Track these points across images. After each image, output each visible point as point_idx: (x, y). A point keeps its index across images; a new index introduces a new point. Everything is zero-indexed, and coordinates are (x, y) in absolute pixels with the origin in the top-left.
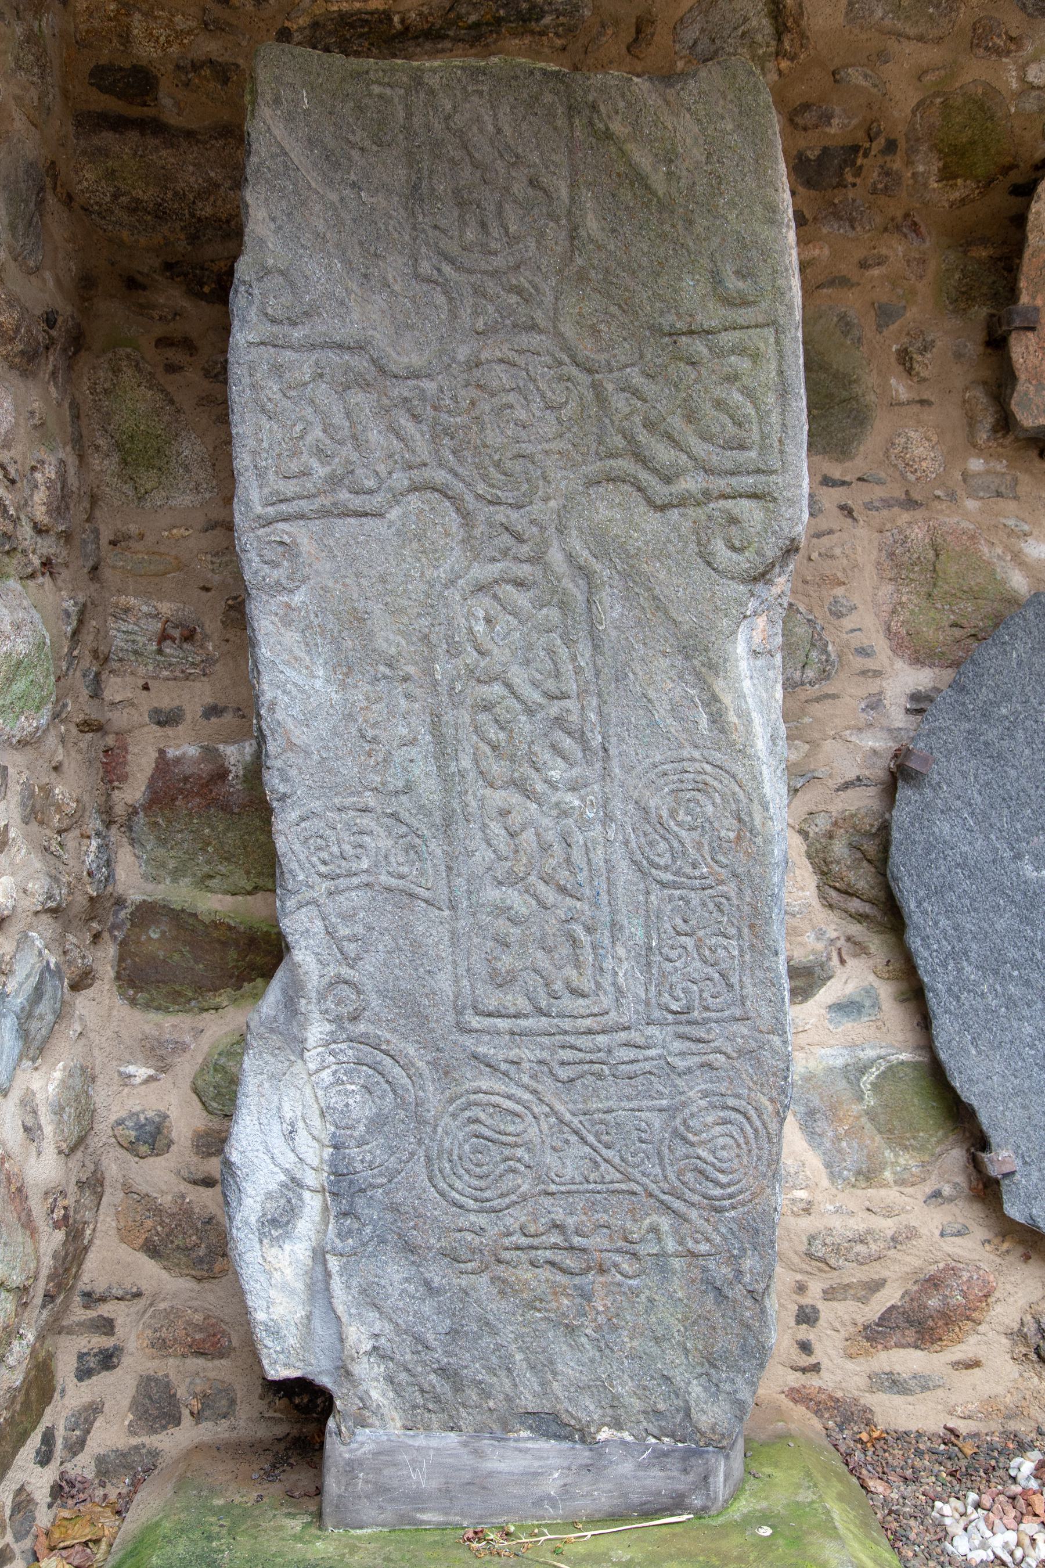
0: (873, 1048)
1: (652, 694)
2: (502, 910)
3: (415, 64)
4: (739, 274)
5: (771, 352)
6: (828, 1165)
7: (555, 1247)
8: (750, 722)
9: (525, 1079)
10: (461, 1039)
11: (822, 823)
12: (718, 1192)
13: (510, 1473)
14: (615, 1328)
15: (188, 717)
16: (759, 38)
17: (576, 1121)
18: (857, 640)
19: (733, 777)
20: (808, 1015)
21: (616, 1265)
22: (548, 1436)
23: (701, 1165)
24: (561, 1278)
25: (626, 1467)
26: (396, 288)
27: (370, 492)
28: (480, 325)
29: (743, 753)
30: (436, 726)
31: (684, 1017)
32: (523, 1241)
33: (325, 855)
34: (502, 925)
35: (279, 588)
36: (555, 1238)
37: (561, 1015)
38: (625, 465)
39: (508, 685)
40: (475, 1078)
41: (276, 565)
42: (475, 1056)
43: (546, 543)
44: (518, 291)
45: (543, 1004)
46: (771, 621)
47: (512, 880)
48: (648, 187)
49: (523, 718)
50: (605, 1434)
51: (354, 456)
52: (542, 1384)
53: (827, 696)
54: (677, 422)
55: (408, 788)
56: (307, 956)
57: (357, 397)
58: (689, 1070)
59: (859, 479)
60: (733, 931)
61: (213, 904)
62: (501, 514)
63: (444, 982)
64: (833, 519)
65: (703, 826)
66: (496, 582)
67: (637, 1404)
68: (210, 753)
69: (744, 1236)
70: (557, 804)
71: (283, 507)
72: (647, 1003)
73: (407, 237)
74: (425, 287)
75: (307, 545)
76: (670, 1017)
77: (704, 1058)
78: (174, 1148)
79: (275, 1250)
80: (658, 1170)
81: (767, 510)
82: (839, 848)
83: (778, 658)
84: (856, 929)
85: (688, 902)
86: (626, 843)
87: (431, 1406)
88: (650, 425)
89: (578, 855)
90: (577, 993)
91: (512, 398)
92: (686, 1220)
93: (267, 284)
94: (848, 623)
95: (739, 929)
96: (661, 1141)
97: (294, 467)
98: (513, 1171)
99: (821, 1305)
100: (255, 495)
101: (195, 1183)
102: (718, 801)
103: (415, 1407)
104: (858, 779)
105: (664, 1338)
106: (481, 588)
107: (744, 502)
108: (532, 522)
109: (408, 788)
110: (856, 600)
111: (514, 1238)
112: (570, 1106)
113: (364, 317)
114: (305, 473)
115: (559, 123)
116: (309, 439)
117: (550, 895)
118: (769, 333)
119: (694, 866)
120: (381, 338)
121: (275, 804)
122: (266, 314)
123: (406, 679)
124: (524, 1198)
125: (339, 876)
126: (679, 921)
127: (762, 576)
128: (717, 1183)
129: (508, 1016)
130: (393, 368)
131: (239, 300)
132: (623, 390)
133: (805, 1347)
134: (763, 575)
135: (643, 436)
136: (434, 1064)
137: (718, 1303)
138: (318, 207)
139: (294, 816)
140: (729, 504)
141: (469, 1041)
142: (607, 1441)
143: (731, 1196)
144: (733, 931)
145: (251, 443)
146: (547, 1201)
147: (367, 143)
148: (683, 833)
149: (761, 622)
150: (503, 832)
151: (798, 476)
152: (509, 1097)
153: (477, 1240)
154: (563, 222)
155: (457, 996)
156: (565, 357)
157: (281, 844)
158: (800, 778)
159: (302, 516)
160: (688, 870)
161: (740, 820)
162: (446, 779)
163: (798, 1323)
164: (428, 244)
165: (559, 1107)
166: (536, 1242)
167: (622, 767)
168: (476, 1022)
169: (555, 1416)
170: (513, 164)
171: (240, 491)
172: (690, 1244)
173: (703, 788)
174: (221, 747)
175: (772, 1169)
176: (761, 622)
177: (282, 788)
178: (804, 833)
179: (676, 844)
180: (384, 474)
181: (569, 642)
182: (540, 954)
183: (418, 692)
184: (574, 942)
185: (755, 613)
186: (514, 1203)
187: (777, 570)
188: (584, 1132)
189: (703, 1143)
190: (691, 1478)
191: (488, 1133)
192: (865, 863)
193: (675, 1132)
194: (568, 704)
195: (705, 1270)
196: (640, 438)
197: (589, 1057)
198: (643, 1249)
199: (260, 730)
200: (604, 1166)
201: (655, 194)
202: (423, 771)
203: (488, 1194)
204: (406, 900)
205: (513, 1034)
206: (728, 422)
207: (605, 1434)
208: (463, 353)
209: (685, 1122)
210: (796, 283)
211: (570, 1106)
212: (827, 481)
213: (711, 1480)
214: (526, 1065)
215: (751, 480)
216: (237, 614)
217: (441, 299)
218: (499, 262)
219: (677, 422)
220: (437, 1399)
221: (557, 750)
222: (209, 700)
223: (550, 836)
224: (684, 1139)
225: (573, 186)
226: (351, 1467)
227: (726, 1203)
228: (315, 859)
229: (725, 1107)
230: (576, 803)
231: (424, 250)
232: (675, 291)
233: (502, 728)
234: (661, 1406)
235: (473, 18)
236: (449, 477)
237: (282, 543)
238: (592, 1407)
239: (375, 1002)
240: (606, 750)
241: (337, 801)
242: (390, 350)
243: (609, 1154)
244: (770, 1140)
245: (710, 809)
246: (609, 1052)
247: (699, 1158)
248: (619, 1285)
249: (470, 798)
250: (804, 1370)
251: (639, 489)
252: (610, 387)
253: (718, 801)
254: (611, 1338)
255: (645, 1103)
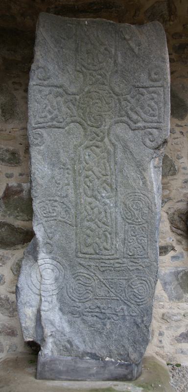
0: (182, 268)
1: (129, 176)
2: (88, 228)
3: (78, 19)
4: (155, 74)
5: (162, 93)
6: (169, 297)
7: (97, 312)
8: (153, 184)
9: (92, 270)
10: (77, 259)
11: (172, 211)
12: (139, 300)
13: (83, 368)
14: (111, 333)
15: (15, 176)
16: (165, 16)
17: (104, 281)
18: (183, 165)
19: (148, 197)
20: (166, 259)
21: (112, 317)
22: (93, 359)
23: (135, 294)
24: (98, 320)
25: (112, 368)
26: (71, 73)
27: (61, 122)
28: (91, 83)
29: (151, 191)
30: (74, 180)
31: (132, 257)
32: (90, 310)
33: (45, 212)
34: (88, 232)
35: (37, 145)
36: (97, 310)
37: (102, 255)
38: (125, 118)
39: (93, 172)
40: (79, 269)
41: (37, 139)
42: (80, 264)
43: (104, 137)
44: (101, 75)
45: (98, 252)
46: (160, 160)
47: (92, 220)
48: (134, 52)
49: (96, 180)
50: (107, 359)
51: (58, 113)
52: (93, 346)
53: (175, 179)
54: (138, 109)
55: (67, 196)
56: (39, 232)
57: (59, 99)
58: (133, 270)
59: (185, 125)
60: (146, 236)
61: (19, 223)
62: (94, 129)
63: (73, 245)
64: (178, 135)
65: (140, 210)
66: (91, 146)
67: (116, 352)
68: (20, 185)
69: (145, 312)
70: (104, 202)
71: (39, 125)
72: (123, 253)
73: (74, 61)
74: (78, 73)
75: (45, 135)
76: (129, 256)
77: (137, 267)
78: (5, 283)
79: (28, 309)
80: (124, 294)
81: (159, 132)
82: (176, 217)
83: (161, 169)
84: (179, 237)
85: (135, 228)
86: (121, 213)
87: (65, 350)
88: (131, 109)
89: (108, 215)
90: (106, 249)
91: (97, 101)
92: (130, 307)
93: (39, 70)
94: (181, 161)
95: (147, 235)
96: (125, 287)
97: (43, 115)
98: (88, 293)
99: (165, 331)
100: (33, 122)
101: (10, 292)
102: (144, 203)
103: (61, 350)
104: (181, 200)
105: (123, 336)
106: (87, 147)
107: (154, 130)
108: (101, 132)
109: (67, 196)
110: (183, 155)
111: (87, 310)
112: (103, 277)
113: (63, 80)
114: (46, 117)
115: (113, 35)
116: (47, 109)
117: (101, 225)
118: (162, 89)
119: (137, 219)
120: (67, 84)
121: (33, 198)
122: (38, 78)
123: (67, 169)
124: (90, 300)
125: (48, 217)
126: (132, 233)
127: (158, 148)
128: (138, 298)
129: (89, 254)
130: (69, 93)
131: (32, 74)
132: (125, 100)
133: (161, 341)
134: (158, 148)
135: (130, 112)
136: (70, 265)
137: (137, 328)
138: (53, 52)
139: (38, 201)
140: (150, 130)
141: (79, 260)
142: (108, 361)
143: (142, 302)
144: (146, 236)
145: (33, 109)
146: (96, 301)
147: (65, 38)
148: (134, 211)
149: (157, 159)
150: (90, 208)
151: (167, 124)
152: (88, 274)
153: (78, 309)
154: (113, 59)
155: (76, 249)
156: (111, 92)
157: (34, 208)
158: (165, 200)
159: (44, 128)
160: (136, 220)
161: (149, 208)
162: (77, 195)
163: (159, 335)
164: (79, 63)
165: (99, 277)
166: (93, 311)
167: (120, 194)
168: (80, 255)
169: (95, 354)
170: (101, 44)
171: (29, 121)
172: (131, 313)
173: (140, 200)
174: (22, 184)
175: (152, 296)
176: (157, 159)
177: (35, 195)
178: (167, 213)
179: (133, 214)
180: (65, 118)
181: (108, 162)
182: (97, 239)
183: (70, 172)
184: (106, 236)
185: (155, 157)
186: (88, 301)
187: (161, 147)
188: (106, 284)
189: (135, 288)
190: (128, 371)
191: (82, 283)
192: (182, 221)
193: (129, 286)
194: (108, 177)
195: (134, 320)
196: (129, 112)
197: (108, 265)
198: (119, 314)
199: (31, 180)
200: (110, 292)
201: (135, 53)
202: (71, 192)
203: (82, 298)
204: (65, 224)
205: (90, 259)
206: (151, 110)
207: (107, 359)
208: (86, 90)
209: (131, 283)
210: (169, 77)
211: (103, 277)
212: (178, 126)
213: (133, 372)
214: (92, 267)
215: (156, 124)
216: (27, 150)
217: (81, 76)
218: (97, 68)
219: (138, 109)
220: (66, 348)
221: (104, 189)
222: (20, 172)
223: (101, 210)
224: (131, 287)
225: (116, 50)
226: (44, 364)
227: (141, 303)
228: (42, 213)
229: (142, 280)
230: (108, 202)
231: (78, 64)
232: (139, 77)
233: (91, 182)
234: (122, 353)
235: (95, 8)
236: (81, 120)
237: (39, 134)
238: (104, 352)
239: (56, 249)
240: (116, 189)
241: (49, 198)
242: (69, 88)
243: (112, 290)
244: (152, 288)
245: (141, 205)
246: (113, 264)
247: (134, 292)
248: (113, 322)
249: (82, 200)
250: (160, 347)
251: (128, 125)
252: (122, 99)
253: (144, 203)
254: (110, 335)
255: (122, 278)
